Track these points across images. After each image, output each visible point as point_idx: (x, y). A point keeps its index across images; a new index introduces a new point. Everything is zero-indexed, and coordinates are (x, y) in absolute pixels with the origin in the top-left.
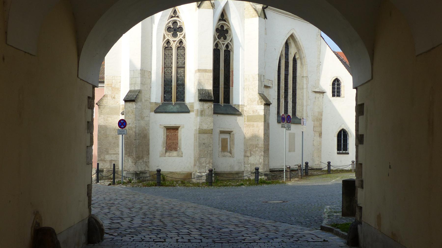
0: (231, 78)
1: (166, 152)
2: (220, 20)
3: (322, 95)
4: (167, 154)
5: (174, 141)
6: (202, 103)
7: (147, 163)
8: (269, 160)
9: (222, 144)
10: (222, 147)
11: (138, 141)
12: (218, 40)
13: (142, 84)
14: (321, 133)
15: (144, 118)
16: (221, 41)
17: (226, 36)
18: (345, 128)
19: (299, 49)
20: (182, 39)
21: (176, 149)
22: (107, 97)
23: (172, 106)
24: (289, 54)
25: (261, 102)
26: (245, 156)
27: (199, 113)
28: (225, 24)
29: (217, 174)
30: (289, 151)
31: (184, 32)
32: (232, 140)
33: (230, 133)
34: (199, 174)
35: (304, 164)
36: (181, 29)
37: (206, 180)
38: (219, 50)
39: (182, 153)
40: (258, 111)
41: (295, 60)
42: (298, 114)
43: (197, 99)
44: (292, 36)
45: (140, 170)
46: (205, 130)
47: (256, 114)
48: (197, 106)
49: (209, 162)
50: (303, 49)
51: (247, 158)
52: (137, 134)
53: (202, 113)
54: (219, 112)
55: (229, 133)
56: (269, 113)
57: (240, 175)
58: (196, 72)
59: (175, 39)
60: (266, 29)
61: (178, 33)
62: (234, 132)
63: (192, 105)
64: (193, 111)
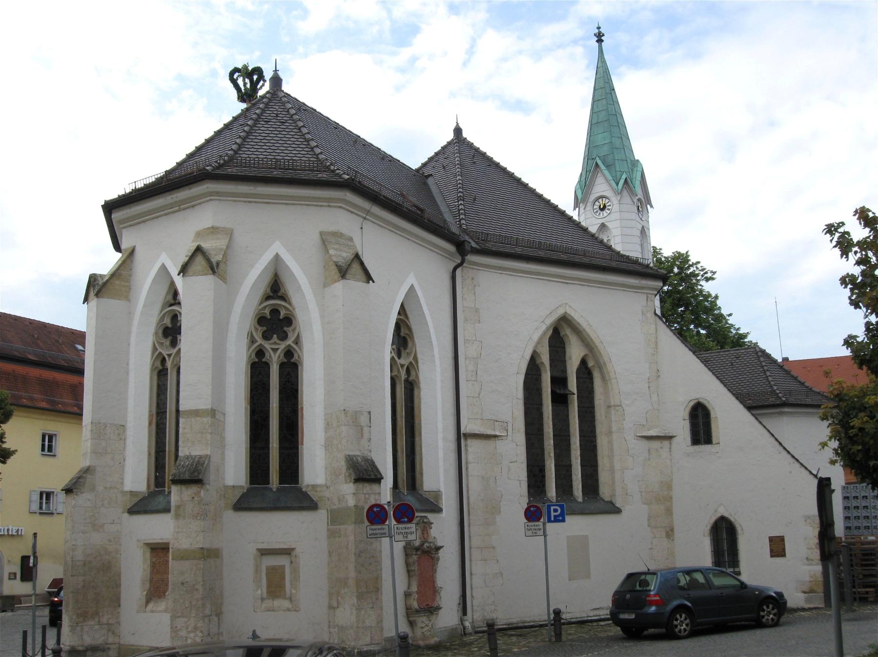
1: (148, 602)
3: (666, 443)
4: (151, 606)
7: (112, 628)
11: (81, 578)
14: (672, 530)
15: (102, 526)
16: (267, 345)
17: (285, 332)
18: (726, 515)
24: (567, 358)
25: (350, 475)
26: (330, 607)
32: (295, 571)
35: (552, 616)
41: (585, 372)
42: (605, 491)
45: (88, 641)
46: (186, 550)
49: (196, 628)
54: (255, 506)
55: (287, 552)
62: (298, 551)
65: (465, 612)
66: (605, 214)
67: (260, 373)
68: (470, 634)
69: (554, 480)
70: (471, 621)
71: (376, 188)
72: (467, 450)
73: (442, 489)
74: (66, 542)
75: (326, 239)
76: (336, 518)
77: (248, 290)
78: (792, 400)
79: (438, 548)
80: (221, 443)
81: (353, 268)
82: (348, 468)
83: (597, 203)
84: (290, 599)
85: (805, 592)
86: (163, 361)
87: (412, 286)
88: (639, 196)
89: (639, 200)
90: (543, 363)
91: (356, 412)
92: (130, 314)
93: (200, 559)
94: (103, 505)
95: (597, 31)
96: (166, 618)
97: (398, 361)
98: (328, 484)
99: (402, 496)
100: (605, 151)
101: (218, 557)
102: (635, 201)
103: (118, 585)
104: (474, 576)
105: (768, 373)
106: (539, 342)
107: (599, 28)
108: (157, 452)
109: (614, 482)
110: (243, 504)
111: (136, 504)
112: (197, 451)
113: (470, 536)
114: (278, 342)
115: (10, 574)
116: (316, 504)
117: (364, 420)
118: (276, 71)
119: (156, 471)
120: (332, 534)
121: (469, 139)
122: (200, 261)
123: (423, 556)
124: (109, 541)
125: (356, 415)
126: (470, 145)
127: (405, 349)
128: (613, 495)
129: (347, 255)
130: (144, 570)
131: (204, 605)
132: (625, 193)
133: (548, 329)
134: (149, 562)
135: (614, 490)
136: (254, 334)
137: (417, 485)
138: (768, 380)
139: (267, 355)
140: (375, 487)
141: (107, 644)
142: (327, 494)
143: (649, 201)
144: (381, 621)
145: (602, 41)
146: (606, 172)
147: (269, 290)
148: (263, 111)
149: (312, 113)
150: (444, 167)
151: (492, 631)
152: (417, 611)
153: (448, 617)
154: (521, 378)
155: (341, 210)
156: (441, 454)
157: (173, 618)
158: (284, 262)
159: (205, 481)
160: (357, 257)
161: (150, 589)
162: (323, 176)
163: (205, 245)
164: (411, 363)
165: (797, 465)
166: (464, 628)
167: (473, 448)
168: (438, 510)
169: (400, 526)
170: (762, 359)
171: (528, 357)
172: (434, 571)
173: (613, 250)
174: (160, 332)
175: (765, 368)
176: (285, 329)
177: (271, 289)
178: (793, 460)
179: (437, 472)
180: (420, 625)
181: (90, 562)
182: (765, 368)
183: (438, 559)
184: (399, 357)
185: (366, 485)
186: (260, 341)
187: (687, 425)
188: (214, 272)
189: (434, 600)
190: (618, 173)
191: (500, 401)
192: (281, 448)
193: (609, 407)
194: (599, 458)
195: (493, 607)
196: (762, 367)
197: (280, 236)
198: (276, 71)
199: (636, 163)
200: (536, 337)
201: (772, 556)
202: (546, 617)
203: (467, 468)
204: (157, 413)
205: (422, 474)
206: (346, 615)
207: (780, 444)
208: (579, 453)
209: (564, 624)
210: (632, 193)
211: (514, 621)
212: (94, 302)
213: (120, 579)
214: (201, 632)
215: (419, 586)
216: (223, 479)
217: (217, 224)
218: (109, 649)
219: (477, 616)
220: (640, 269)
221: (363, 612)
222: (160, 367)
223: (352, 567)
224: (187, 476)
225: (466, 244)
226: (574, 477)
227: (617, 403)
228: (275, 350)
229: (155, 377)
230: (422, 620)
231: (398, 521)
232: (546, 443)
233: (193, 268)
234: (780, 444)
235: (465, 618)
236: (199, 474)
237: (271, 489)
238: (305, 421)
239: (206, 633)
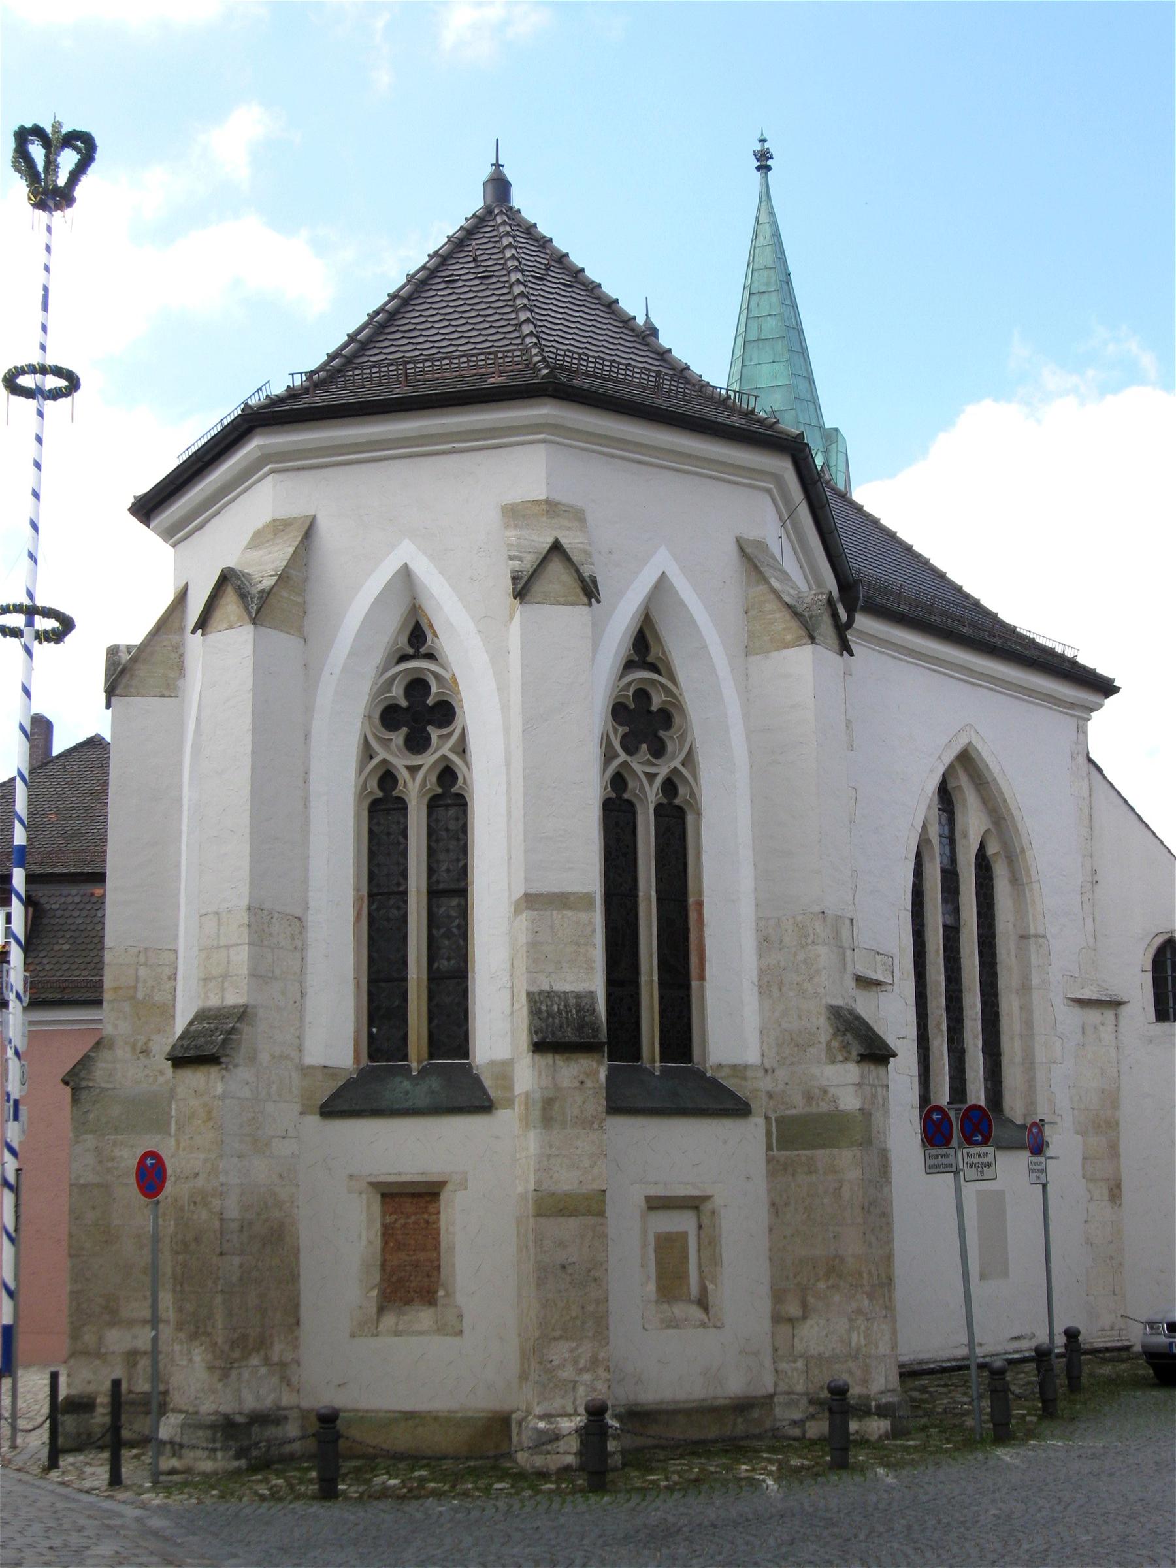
0: (693, 936)
1: (381, 1310)
2: (629, 665)
3: (1109, 1014)
4: (389, 1320)
5: (422, 1256)
6: (549, 1059)
7: (283, 1370)
8: (894, 1333)
9: (659, 1263)
10: (660, 1277)
11: (237, 1260)
12: (623, 756)
13: (259, 976)
14: (1119, 1186)
16: (638, 765)
19: (998, 814)
20: (455, 758)
21: (428, 1296)
22: (111, 1046)
23: (407, 1084)
25: (845, 1047)
26: (777, 1319)
27: (536, 1113)
28: (653, 681)
29: (638, 1416)
30: (983, 1277)
31: (457, 724)
33: (697, 1208)
34: (541, 1425)
35: (1061, 1340)
36: (445, 712)
37: (579, 1454)
38: (631, 805)
39: (460, 1316)
40: (832, 1090)
42: (1014, 1106)
43: (524, 1040)
44: (966, 759)
45: (250, 1403)
47: (824, 1107)
48: (527, 1075)
50: (1015, 813)
51: (785, 1329)
52: (234, 1226)
53: (548, 1112)
55: (694, 1204)
56: (886, 1100)
57: (756, 1414)
58: (517, 911)
59: (416, 760)
60: (848, 724)
61: (434, 733)
62: (718, 1201)
63: (504, 1070)
64: (509, 1103)
103: (294, 1278)
116: (747, 1105)
118: (497, 165)
120: (775, 1168)
124: (281, 1177)
130: (371, 1243)
134: (378, 1225)
136: (612, 736)
141: (279, 1408)
145: (769, 168)
147: (404, 640)
158: (677, 593)
181: (251, 1223)
198: (497, 165)
208: (980, 1028)
217: (557, 497)
218: (286, 1418)
224: (570, 1036)
227: (1041, 931)
228: (413, 770)
233: (538, 588)
238: (708, 931)
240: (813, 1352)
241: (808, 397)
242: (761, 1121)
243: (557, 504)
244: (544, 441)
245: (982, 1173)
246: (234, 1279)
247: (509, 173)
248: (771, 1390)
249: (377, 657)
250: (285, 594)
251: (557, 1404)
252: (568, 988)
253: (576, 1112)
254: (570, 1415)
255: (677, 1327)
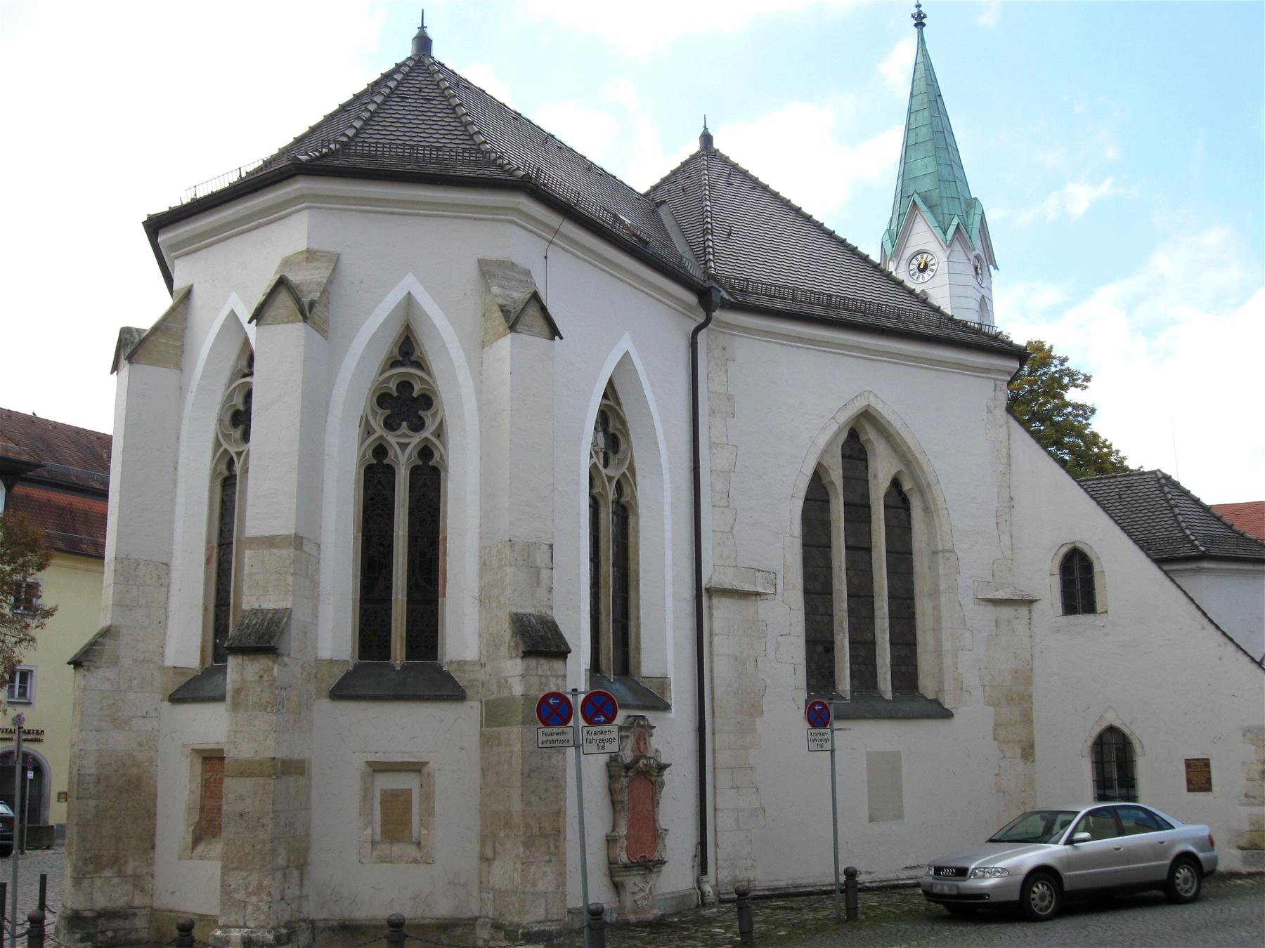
1: (196, 842)
3: (1023, 611)
4: (200, 848)
7: (138, 882)
11: (92, 803)
14: (1032, 746)
16: (392, 439)
17: (421, 418)
18: (1117, 724)
32: (428, 798)
35: (843, 878)
41: (899, 500)
42: (927, 684)
45: (101, 902)
47: (506, 694)
49: (260, 888)
54: (363, 692)
55: (416, 768)
57: (459, 932)
62: (432, 767)
65: (703, 869)
66: (927, 278)
67: (379, 483)
68: (712, 905)
69: (848, 665)
70: (713, 882)
71: (572, 199)
72: (711, 615)
73: (671, 675)
74: (73, 745)
75: (489, 271)
76: (494, 714)
77: (362, 348)
78: (1215, 551)
79: (662, 768)
80: (314, 593)
81: (530, 314)
82: (514, 634)
83: (914, 261)
84: (419, 844)
85: (1242, 848)
86: (231, 463)
87: (627, 355)
88: (977, 252)
89: (977, 257)
90: (832, 483)
91: (529, 545)
92: (181, 390)
93: (269, 776)
94: (130, 688)
95: (915, 11)
96: (215, 867)
97: (604, 471)
98: (484, 660)
99: (605, 683)
100: (926, 185)
101: (302, 774)
102: (972, 258)
104: (719, 814)
105: (1177, 511)
106: (826, 451)
107: (918, 6)
108: (217, 606)
109: (941, 670)
110: (345, 690)
111: (182, 688)
112: (272, 602)
113: (714, 750)
114: (411, 433)
115: (60, 794)
116: (463, 691)
117: (541, 557)
118: (423, 27)
119: (216, 636)
120: (487, 741)
121: (722, 151)
122: (286, 298)
123: (636, 779)
125: (529, 549)
126: (725, 160)
127: (615, 453)
128: (940, 691)
129: (520, 295)
130: (192, 792)
131: (274, 850)
132: (957, 246)
133: (840, 430)
135: (941, 683)
137: (632, 667)
138: (1176, 520)
139: (391, 453)
140: (557, 665)
141: (131, 907)
142: (481, 676)
143: (991, 260)
144: (564, 884)
145: (924, 25)
146: (928, 215)
148: (400, 83)
149: (477, 93)
150: (684, 190)
151: (744, 900)
152: (626, 867)
153: (676, 877)
154: (799, 504)
155: (513, 227)
156: (670, 617)
157: (226, 870)
159: (282, 650)
160: (535, 297)
161: (199, 822)
162: (487, 172)
163: (294, 277)
164: (624, 475)
165: (1231, 647)
166: (703, 894)
167: (721, 614)
168: (662, 705)
169: (593, 729)
170: (1166, 489)
171: (809, 471)
172: (655, 803)
173: (943, 314)
174: (228, 418)
175: (1173, 502)
176: (421, 413)
177: (400, 349)
178: (1225, 640)
179: (663, 647)
180: (630, 887)
181: (107, 777)
182: (1173, 502)
183: (662, 784)
184: (606, 466)
185: (542, 661)
186: (379, 431)
187: (1056, 583)
188: (305, 319)
189: (654, 849)
190: (947, 217)
191: (764, 537)
192: (411, 601)
193: (935, 553)
194: (919, 633)
195: (749, 862)
196: (1168, 501)
197: (417, 265)
198: (423, 27)
199: (972, 203)
200: (822, 441)
201: (1190, 790)
202: (832, 879)
203: (711, 643)
204: (220, 545)
205: (638, 649)
206: (504, 873)
207: (1204, 614)
208: (887, 624)
209: (860, 890)
210: (967, 247)
211: (782, 884)
212: (125, 368)
213: (155, 805)
214: (270, 894)
215: (630, 826)
216: (315, 648)
217: (315, 247)
219: (722, 874)
220: (984, 340)
221: (533, 868)
222: (226, 473)
223: (516, 792)
224: (252, 642)
225: (714, 293)
226: (879, 661)
227: (948, 547)
228: (403, 446)
229: (218, 489)
230: (633, 881)
231: (590, 720)
232: (836, 607)
233: (270, 313)
234: (1204, 614)
235: (705, 878)
236: (271, 637)
237: (393, 667)
238: (448, 560)
239: (277, 897)
240: (497, 887)
241: (951, 178)
242: (476, 704)
243: (316, 252)
244: (308, 208)
245: (603, 747)
246: (89, 816)
247: (430, 33)
248: (477, 914)
249: (224, 378)
250: (163, 340)
251: (232, 919)
252: (272, 606)
253: (256, 699)
254: (240, 927)
255: (391, 862)
